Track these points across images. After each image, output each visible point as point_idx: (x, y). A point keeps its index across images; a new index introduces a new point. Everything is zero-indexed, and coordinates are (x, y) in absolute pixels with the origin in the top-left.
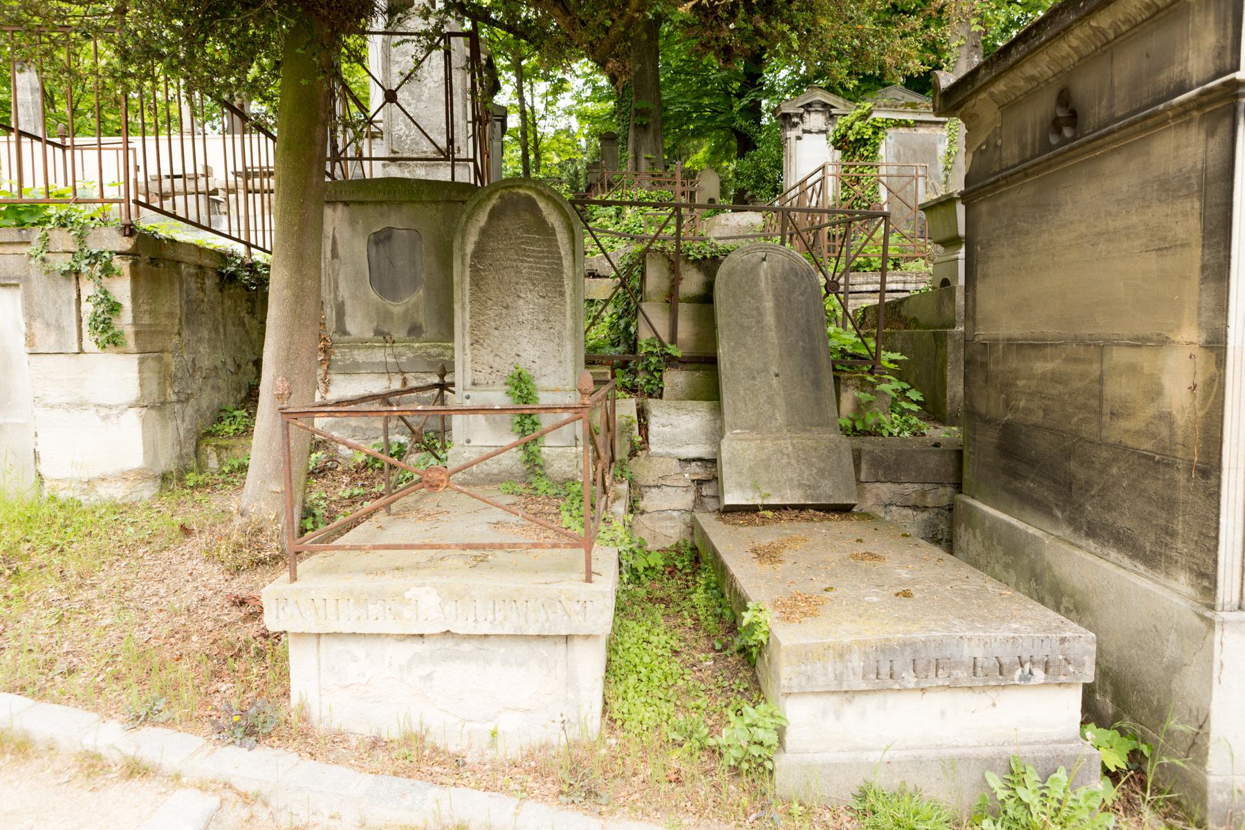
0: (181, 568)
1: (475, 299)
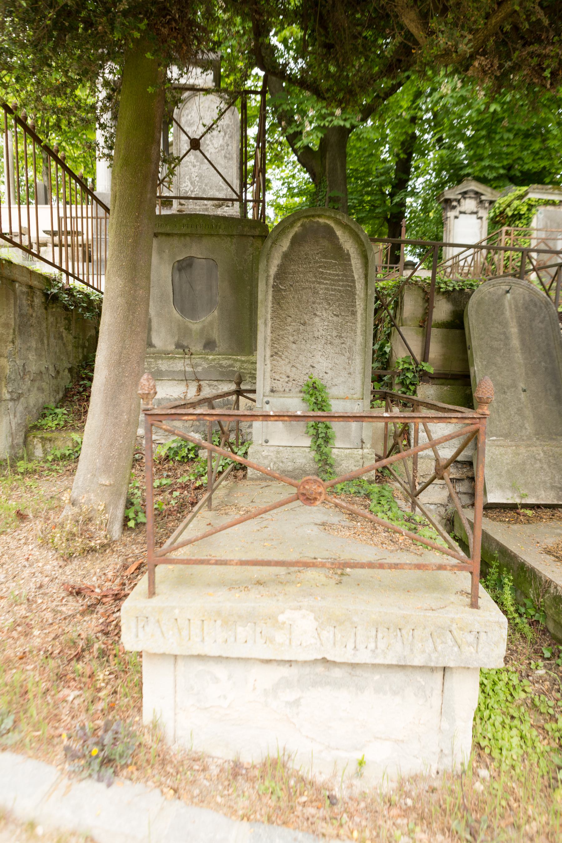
0: (18, 553)
1: (276, 316)
